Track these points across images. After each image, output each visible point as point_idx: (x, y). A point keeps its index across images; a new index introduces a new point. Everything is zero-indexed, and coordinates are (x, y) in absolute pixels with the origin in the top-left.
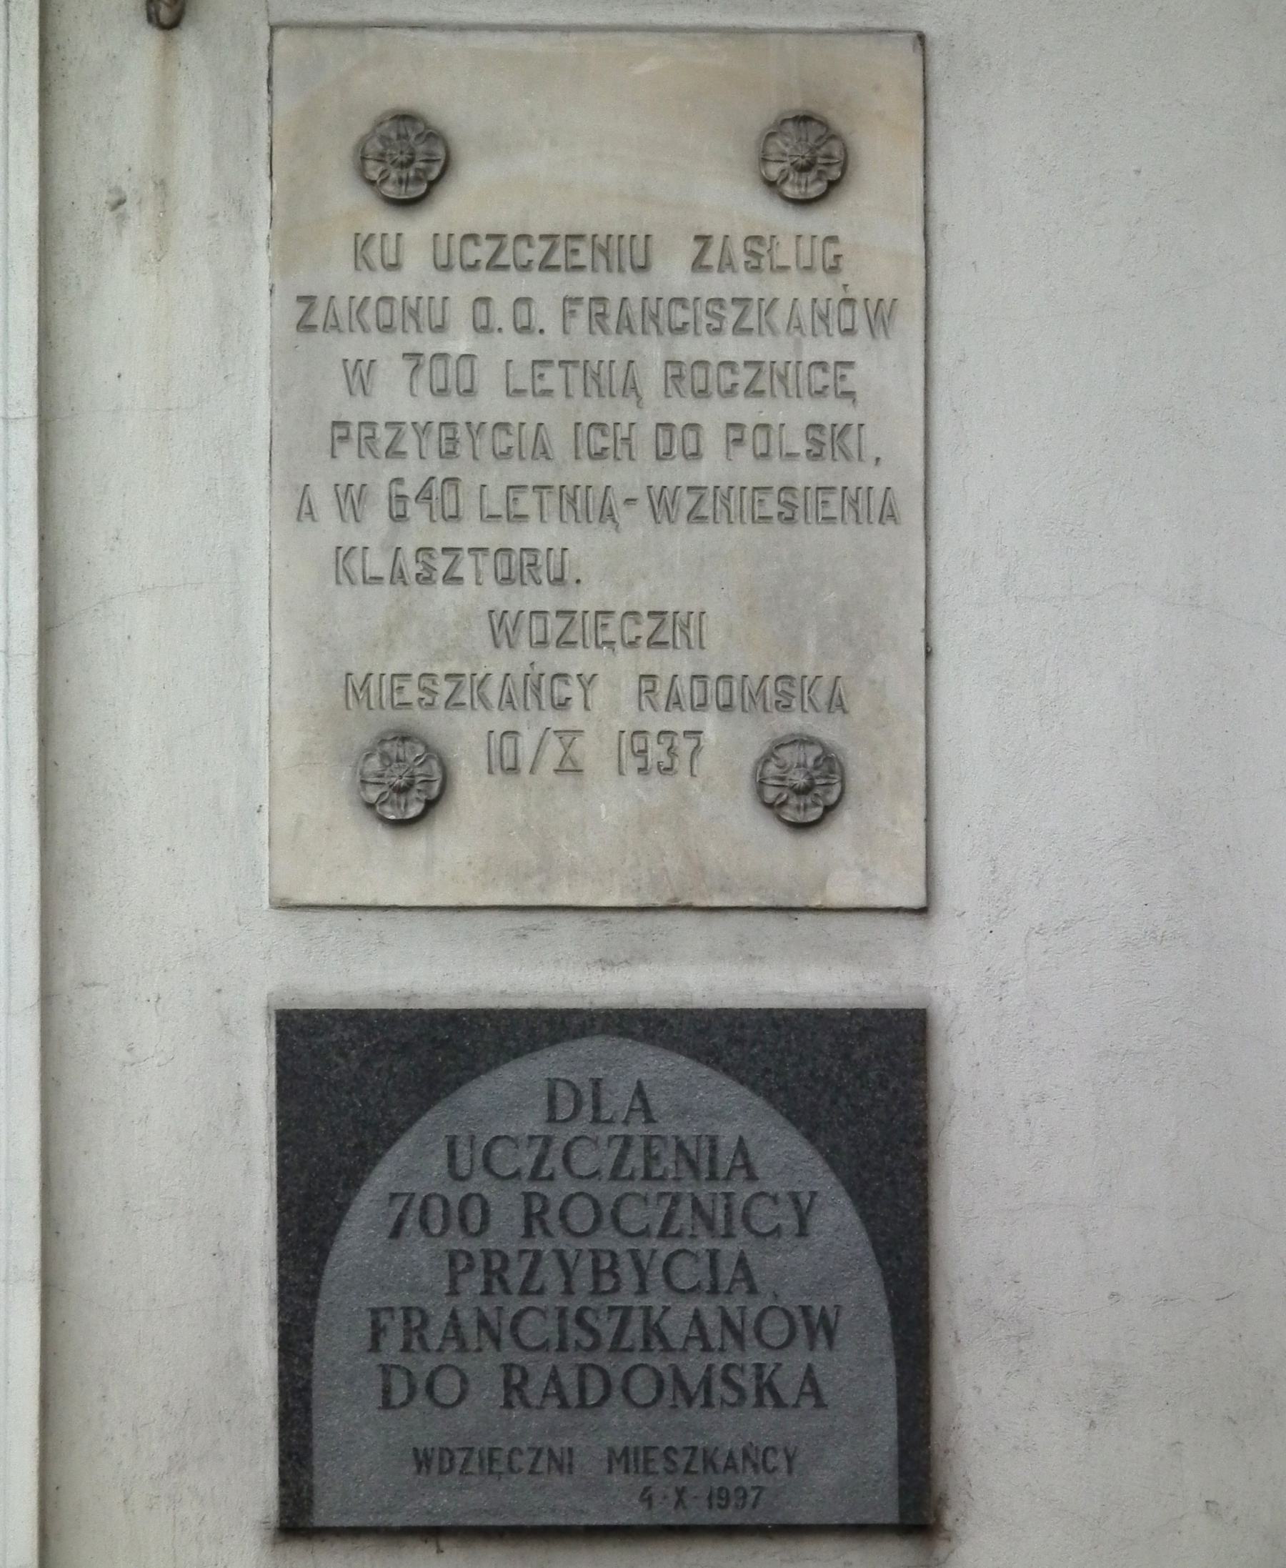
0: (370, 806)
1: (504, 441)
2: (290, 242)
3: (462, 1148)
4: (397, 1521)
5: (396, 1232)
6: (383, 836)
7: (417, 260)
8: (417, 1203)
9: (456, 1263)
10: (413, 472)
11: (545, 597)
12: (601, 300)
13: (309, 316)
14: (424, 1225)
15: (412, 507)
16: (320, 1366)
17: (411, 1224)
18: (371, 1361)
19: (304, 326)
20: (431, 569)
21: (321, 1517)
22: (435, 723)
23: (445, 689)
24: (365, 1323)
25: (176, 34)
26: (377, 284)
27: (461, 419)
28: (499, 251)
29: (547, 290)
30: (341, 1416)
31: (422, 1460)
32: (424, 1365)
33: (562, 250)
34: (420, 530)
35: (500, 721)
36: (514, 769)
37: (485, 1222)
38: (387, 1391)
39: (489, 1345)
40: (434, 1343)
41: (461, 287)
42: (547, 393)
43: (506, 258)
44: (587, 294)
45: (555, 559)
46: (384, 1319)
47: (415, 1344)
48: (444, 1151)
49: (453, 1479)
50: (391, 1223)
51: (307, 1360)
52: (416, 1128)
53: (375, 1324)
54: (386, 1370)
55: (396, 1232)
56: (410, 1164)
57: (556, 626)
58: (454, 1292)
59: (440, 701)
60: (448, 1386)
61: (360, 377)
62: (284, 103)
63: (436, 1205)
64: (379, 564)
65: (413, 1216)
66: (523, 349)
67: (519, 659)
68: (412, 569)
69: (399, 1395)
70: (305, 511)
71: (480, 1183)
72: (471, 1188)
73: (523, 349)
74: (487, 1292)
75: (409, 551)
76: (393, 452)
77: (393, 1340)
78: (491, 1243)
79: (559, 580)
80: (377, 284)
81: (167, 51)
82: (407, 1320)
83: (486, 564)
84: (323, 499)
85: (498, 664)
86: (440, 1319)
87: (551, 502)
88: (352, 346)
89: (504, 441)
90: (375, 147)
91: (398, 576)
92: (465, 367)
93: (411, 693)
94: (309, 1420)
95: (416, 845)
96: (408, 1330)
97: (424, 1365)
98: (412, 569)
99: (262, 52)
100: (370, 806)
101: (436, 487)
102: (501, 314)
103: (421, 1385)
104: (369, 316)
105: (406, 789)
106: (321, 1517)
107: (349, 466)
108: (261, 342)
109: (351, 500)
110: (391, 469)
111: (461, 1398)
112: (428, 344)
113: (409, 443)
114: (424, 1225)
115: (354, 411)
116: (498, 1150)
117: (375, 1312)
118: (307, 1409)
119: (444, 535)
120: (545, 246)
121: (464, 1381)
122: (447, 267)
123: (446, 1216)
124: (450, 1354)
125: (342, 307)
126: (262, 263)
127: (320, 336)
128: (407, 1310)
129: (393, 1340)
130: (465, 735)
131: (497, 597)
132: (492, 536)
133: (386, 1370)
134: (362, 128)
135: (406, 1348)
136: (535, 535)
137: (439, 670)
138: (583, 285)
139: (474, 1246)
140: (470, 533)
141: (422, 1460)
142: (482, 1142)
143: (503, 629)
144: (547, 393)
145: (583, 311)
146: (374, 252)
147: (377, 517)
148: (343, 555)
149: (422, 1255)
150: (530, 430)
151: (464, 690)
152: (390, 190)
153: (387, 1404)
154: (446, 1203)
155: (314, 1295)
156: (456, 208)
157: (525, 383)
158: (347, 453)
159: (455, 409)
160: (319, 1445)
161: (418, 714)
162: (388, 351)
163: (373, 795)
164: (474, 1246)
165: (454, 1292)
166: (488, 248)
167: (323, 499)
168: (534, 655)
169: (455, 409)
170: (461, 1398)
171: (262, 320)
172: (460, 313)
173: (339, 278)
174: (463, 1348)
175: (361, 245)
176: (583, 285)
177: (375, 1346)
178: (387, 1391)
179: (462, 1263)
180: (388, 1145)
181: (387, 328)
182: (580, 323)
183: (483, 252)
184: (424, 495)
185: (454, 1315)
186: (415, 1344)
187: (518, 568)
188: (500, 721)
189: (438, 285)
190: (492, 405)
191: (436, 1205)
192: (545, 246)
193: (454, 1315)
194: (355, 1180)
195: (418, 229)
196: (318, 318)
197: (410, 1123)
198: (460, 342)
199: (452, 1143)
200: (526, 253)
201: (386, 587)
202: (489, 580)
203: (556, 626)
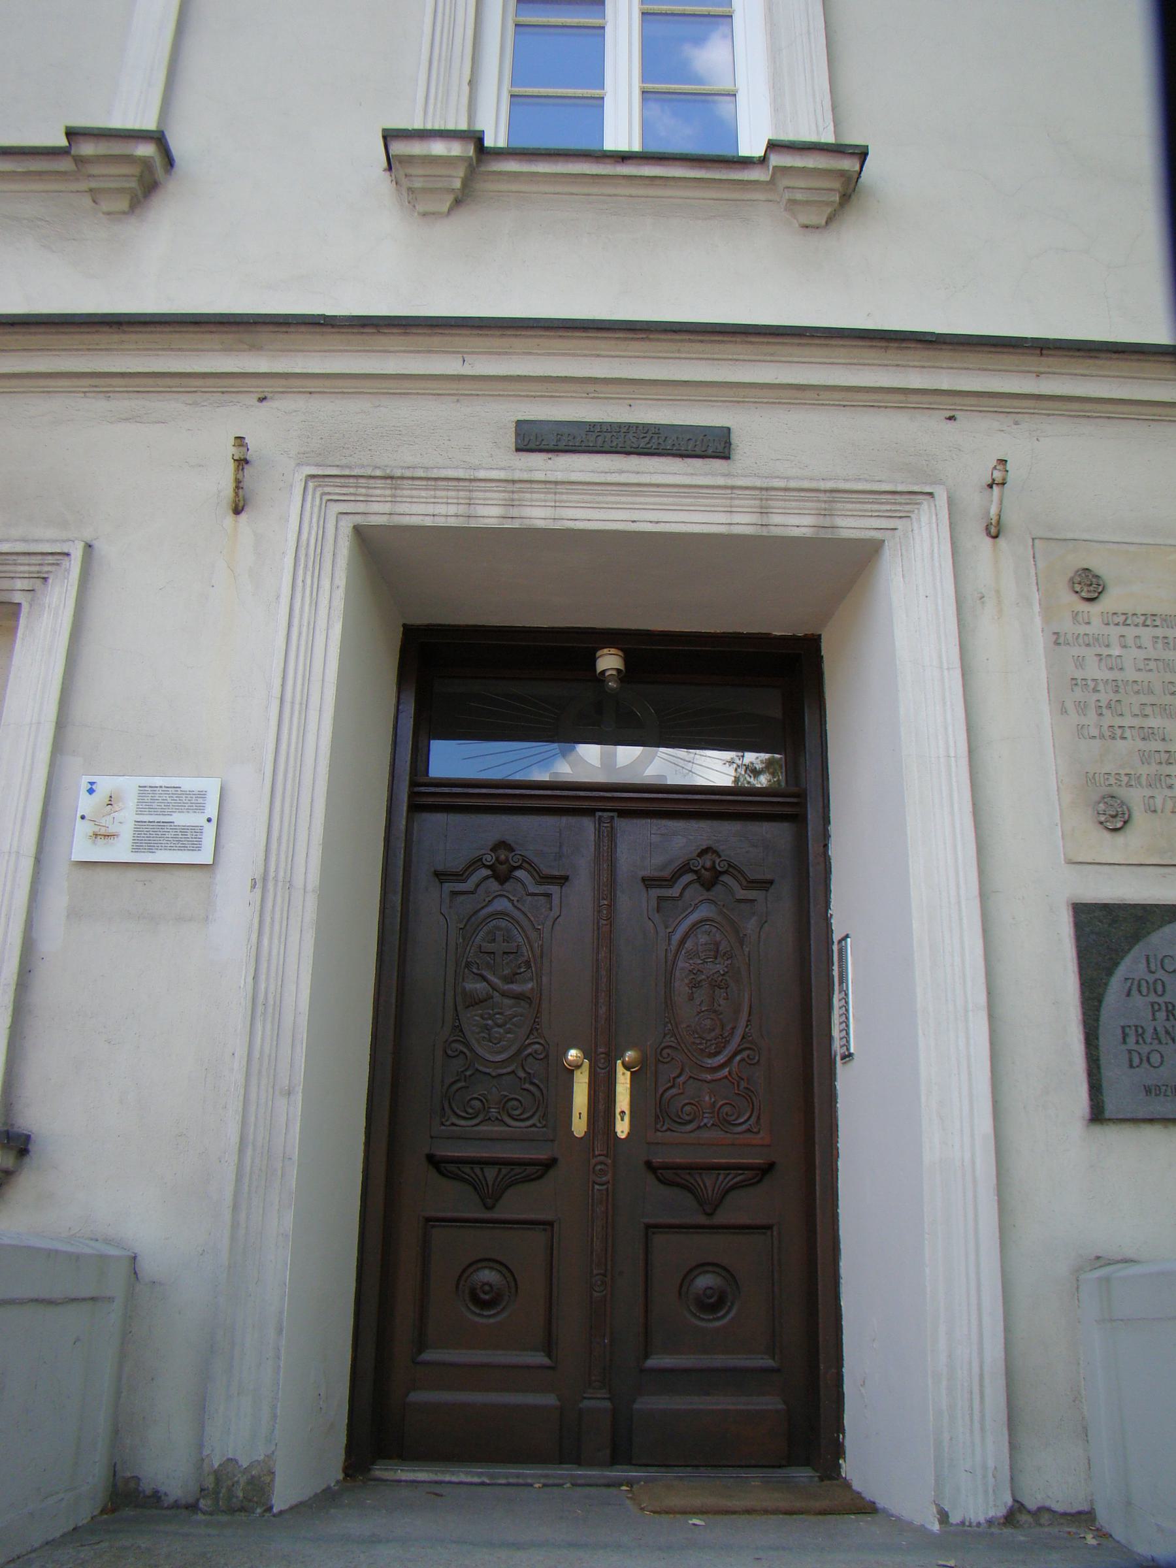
0: (1101, 823)
1: (1136, 688)
2: (1048, 612)
3: (1152, 960)
4: (1140, 1115)
5: (1128, 994)
6: (1107, 835)
7: (1096, 621)
8: (1136, 983)
9: (1154, 1008)
10: (1104, 697)
11: (1160, 746)
12: (1165, 638)
13: (1057, 639)
14: (1140, 991)
15: (1104, 711)
16: (1102, 1049)
17: (1134, 992)
18: (1124, 1047)
19: (1057, 643)
20: (1115, 734)
21: (1107, 1115)
22: (1122, 792)
23: (1125, 779)
24: (1119, 1031)
25: (997, 540)
26: (1082, 629)
27: (1119, 678)
28: (1126, 619)
29: (1146, 634)
30: (1113, 1071)
31: (1148, 1090)
32: (1145, 1049)
33: (1149, 619)
34: (1109, 719)
35: (1148, 792)
36: (1155, 811)
37: (1164, 991)
38: (1131, 1061)
39: (1170, 1042)
40: (1148, 1040)
41: (1114, 632)
42: (1150, 670)
43: (1129, 622)
44: (1161, 635)
45: (1161, 731)
46: (1127, 1030)
47: (1141, 1041)
48: (1144, 961)
49: (1162, 1098)
50: (1126, 991)
51: (1097, 1047)
52: (1132, 952)
53: (1123, 1032)
54: (1130, 1051)
55: (1128, 994)
56: (1131, 966)
57: (1164, 756)
58: (1154, 1019)
59: (1123, 783)
60: (1155, 1058)
61: (1080, 662)
62: (1040, 565)
63: (1144, 983)
64: (1094, 732)
65: (1135, 988)
66: (1141, 655)
67: (1153, 769)
68: (1107, 734)
69: (1136, 1061)
70: (1064, 711)
71: (1160, 974)
72: (1157, 976)
73: (1141, 655)
74: (1168, 1019)
75: (1105, 728)
76: (1095, 690)
77: (1131, 1039)
78: (1166, 998)
79: (1164, 739)
80: (1082, 629)
81: (994, 545)
82: (1137, 1031)
83: (1135, 732)
84: (1070, 706)
85: (1144, 770)
86: (1150, 1031)
87: (1157, 709)
88: (1076, 651)
89: (1136, 688)
90: (1078, 579)
91: (1102, 737)
92: (1119, 660)
93: (1112, 781)
94: (1100, 1073)
95: (1119, 839)
96: (1137, 1035)
97: (1145, 1049)
98: (1107, 734)
99: (1030, 547)
100: (1101, 823)
101: (1113, 703)
102: (1130, 641)
103: (1145, 1058)
104: (1080, 640)
105: (1115, 818)
106: (778, 175)
107: (1078, 694)
108: (1040, 650)
109: (1081, 707)
110: (1095, 697)
111: (1161, 1063)
112: (1105, 652)
113: (1101, 687)
114: (1140, 991)
115: (1079, 675)
116: (1166, 961)
117: (1123, 1028)
118: (1099, 1067)
119: (1118, 721)
120: (1143, 618)
121: (1162, 1057)
122: (1108, 624)
123: (1148, 988)
124: (1156, 1046)
125: (1069, 637)
126: (1038, 621)
127: (1011, 477)
128: (1136, 1026)
129: (1131, 1039)
130: (1135, 797)
131: (1141, 745)
132: (1136, 722)
133: (1130, 1051)
134: (1071, 574)
135: (1137, 1042)
136: (1154, 722)
137: (1122, 772)
138: (1159, 632)
139: (1160, 1000)
140: (1127, 721)
141: (1148, 1090)
142: (1160, 957)
143: (1145, 757)
144: (1150, 670)
145: (1160, 641)
146: (1080, 618)
147: (1092, 714)
148: (1081, 728)
149: (1139, 1002)
150: (1146, 683)
151: (1132, 780)
152: (1084, 594)
153: (1131, 1066)
154: (1156, 992)
155: (1097, 1020)
156: (1108, 603)
157: (1142, 667)
158: (1078, 690)
159: (1116, 675)
160: (1105, 1084)
161: (1115, 788)
162: (1089, 653)
163: (1102, 818)
164: (1160, 1000)
165: (1154, 1019)
166: (1122, 618)
167: (1070, 706)
168: (1158, 767)
169: (1116, 675)
170: (1161, 1063)
171: (1040, 642)
172: (1114, 640)
173: (1067, 626)
174: (1160, 1042)
175: (1075, 615)
176: (1159, 632)
177: (1124, 1042)
178: (1131, 1061)
179: (1156, 1007)
180: (1122, 958)
181: (1088, 645)
182: (1160, 646)
183: (1121, 619)
184: (1109, 707)
185: (1155, 1029)
186: (1141, 1041)
187: (1147, 735)
188: (1148, 792)
189: (1106, 630)
190: (1130, 674)
191: (1144, 983)
192: (1143, 618)
193: (1155, 1029)
194: (1110, 972)
195: (1095, 609)
196: (1061, 640)
197: (1129, 950)
198: (1116, 651)
199: (1147, 957)
200: (1137, 621)
201: (1098, 740)
202: (1138, 739)
203: (1164, 756)
